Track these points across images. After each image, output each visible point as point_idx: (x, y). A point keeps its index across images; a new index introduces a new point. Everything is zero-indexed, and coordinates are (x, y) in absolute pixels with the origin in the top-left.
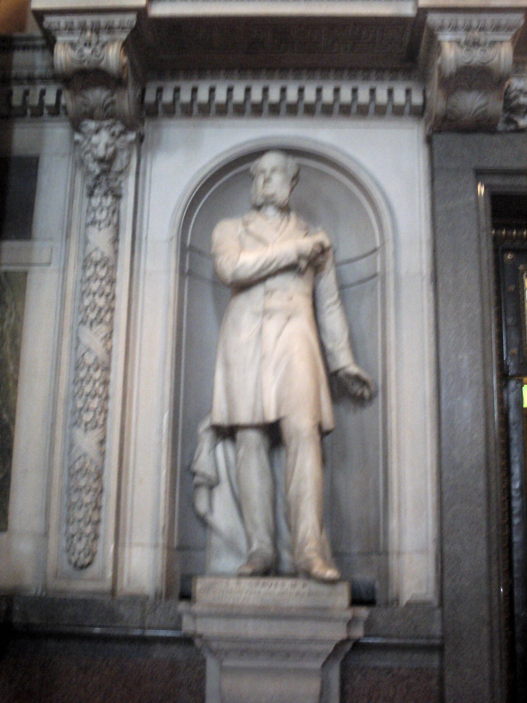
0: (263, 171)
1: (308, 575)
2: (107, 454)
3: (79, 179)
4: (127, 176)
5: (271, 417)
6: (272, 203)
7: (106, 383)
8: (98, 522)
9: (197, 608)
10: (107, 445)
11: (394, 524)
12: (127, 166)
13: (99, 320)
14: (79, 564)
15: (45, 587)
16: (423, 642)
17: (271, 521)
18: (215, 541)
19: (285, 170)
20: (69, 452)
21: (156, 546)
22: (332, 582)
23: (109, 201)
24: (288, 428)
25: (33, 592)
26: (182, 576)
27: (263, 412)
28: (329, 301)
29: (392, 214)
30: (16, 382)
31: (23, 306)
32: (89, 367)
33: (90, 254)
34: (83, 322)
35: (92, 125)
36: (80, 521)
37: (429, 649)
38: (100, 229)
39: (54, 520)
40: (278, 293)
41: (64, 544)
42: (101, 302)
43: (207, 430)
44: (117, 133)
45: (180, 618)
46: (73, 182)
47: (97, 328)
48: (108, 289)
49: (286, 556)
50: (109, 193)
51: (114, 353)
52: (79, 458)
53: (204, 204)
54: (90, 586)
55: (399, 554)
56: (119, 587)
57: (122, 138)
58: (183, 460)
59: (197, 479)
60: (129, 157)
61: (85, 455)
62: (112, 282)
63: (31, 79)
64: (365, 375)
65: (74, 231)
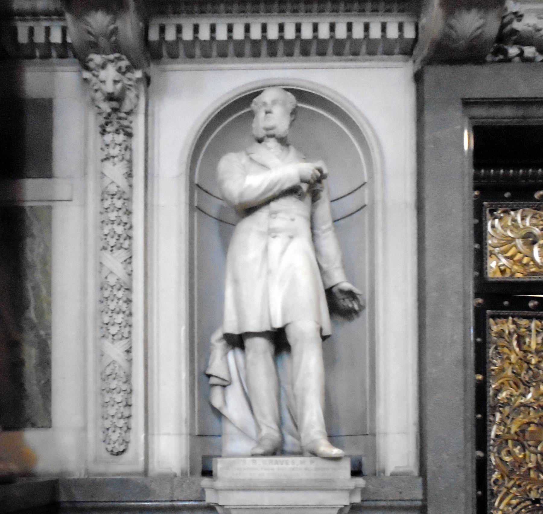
0: (265, 104)
1: (314, 454)
2: (134, 361)
4: (136, 114)
5: (278, 324)
6: (273, 136)
7: (129, 301)
8: (129, 417)
9: (219, 484)
10: (134, 354)
11: (380, 411)
12: (136, 106)
13: (119, 245)
14: (115, 451)
15: (87, 471)
16: (408, 504)
17: (277, 411)
18: (229, 428)
19: (284, 104)
20: (100, 361)
23: (121, 138)
24: (292, 336)
25: (77, 476)
27: (270, 320)
28: (324, 227)
30: (49, 304)
31: (50, 240)
32: (112, 287)
33: (107, 187)
34: (104, 248)
35: (97, 59)
36: (113, 416)
38: (114, 164)
39: (91, 416)
40: (281, 215)
41: (101, 436)
42: (119, 229)
43: (219, 340)
44: (124, 70)
45: (203, 490)
47: (117, 253)
48: (125, 219)
49: (289, 439)
50: (121, 131)
52: (109, 365)
55: (385, 434)
56: (150, 467)
57: (129, 75)
58: (199, 367)
59: (213, 381)
60: (137, 97)
61: (114, 362)
62: (129, 213)
63: (35, 15)
64: (356, 290)
65: (91, 169)
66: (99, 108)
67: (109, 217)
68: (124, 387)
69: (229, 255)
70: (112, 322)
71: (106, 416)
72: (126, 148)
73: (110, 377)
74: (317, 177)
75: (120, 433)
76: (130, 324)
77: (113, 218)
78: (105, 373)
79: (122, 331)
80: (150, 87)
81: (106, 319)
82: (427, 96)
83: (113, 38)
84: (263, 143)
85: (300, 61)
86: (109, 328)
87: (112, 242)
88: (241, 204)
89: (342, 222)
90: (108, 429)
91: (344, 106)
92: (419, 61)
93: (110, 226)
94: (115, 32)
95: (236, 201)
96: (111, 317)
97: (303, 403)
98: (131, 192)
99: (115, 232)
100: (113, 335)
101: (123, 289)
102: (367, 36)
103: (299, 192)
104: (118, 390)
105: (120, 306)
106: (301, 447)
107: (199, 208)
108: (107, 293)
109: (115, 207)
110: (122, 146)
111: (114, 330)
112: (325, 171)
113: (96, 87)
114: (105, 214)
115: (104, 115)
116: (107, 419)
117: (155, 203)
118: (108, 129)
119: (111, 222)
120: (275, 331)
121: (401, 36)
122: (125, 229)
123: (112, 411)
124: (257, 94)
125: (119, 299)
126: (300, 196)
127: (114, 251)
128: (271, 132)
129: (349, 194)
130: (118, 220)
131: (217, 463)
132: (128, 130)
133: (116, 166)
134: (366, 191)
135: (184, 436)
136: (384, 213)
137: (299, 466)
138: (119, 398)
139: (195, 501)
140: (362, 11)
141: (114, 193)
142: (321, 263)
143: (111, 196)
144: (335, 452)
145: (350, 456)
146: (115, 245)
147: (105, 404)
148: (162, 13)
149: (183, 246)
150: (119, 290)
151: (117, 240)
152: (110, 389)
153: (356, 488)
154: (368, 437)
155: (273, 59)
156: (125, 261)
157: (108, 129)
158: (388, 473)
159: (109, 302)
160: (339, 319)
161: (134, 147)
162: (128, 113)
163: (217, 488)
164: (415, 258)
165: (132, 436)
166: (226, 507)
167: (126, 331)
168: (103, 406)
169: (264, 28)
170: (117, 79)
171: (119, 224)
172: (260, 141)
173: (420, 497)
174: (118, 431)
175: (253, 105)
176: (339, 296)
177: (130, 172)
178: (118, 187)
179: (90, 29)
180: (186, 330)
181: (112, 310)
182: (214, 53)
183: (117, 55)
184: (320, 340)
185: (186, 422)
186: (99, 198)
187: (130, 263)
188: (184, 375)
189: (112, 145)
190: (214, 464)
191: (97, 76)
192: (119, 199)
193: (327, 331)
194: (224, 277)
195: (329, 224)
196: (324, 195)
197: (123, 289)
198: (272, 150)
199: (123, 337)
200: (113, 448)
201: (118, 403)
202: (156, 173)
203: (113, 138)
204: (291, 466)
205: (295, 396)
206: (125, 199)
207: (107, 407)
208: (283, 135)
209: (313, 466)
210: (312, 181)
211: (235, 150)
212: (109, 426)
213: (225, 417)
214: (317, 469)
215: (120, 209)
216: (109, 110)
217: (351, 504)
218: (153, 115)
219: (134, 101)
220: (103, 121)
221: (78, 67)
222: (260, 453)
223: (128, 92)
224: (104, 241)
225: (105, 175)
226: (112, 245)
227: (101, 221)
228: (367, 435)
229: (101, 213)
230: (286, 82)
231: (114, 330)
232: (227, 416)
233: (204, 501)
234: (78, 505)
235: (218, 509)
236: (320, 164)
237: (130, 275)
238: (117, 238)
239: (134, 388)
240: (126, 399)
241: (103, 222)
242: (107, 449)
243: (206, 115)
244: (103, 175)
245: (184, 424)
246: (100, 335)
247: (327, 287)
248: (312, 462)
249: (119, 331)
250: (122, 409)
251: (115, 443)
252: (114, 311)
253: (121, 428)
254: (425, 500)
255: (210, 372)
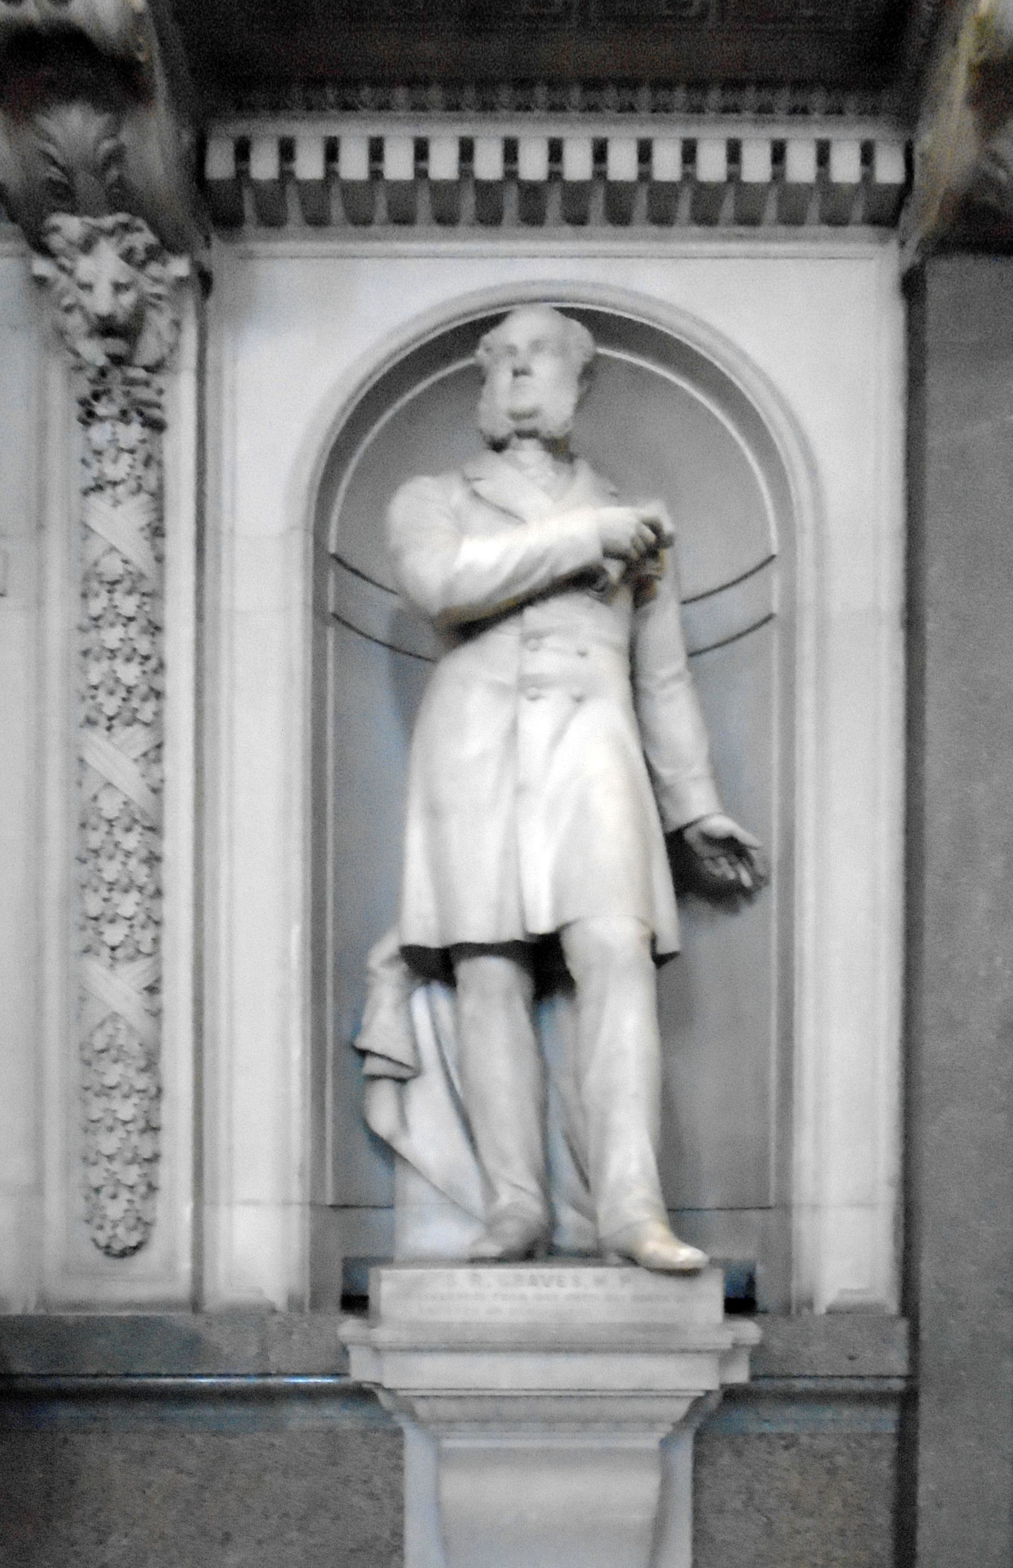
0: (512, 350)
1: (630, 1259)
3: (56, 378)
4: (176, 372)
5: (542, 924)
6: (532, 434)
7: (153, 860)
8: (154, 1159)
9: (383, 1335)
11: (804, 1150)
12: (174, 348)
13: (127, 715)
14: (117, 1247)
15: (43, 1300)
16: (869, 1385)
18: (413, 1189)
19: (562, 351)
21: (286, 1203)
22: (687, 1273)
23: (133, 433)
26: (346, 1260)
27: (522, 914)
28: (664, 673)
29: (813, 470)
32: (110, 822)
33: (96, 564)
34: (90, 722)
36: (110, 1158)
37: (882, 1398)
40: (550, 642)
41: (81, 1206)
42: (130, 673)
43: (391, 961)
44: (140, 256)
46: (43, 385)
47: (122, 733)
48: (144, 645)
49: (568, 1216)
50: (134, 415)
51: (169, 791)
52: (101, 1025)
53: (357, 472)
54: (143, 1292)
55: (815, 1207)
56: (208, 1287)
58: (337, 1030)
59: (373, 1065)
60: (177, 324)
61: (115, 1016)
62: (155, 629)
64: (744, 836)
65: (55, 514)
66: (77, 354)
67: (103, 641)
68: (142, 1082)
69: (417, 746)
70: (110, 913)
71: (92, 1157)
72: (148, 462)
73: (104, 1055)
74: (646, 543)
75: (130, 1201)
76: (156, 918)
77: (112, 643)
78: (92, 1045)
79: (137, 937)
80: (211, 303)
81: (94, 905)
82: (930, 338)
83: (113, 173)
84: (508, 453)
85: (606, 238)
86: (101, 930)
87: (111, 705)
88: (446, 613)
89: (706, 657)
90: (97, 1190)
91: (721, 359)
92: (912, 244)
93: (105, 665)
94: (116, 157)
95: (436, 607)
96: (105, 900)
97: (604, 1131)
98: (161, 576)
99: (117, 680)
100: (113, 949)
101: (138, 829)
102: (778, 175)
103: (601, 583)
104: (125, 1088)
105: (131, 872)
106: (598, 1241)
107: (336, 617)
108: (95, 839)
109: (119, 615)
110: (136, 456)
111: (114, 934)
112: (668, 527)
113: (67, 301)
114: (93, 634)
115: (91, 373)
116: (95, 1164)
117: (225, 603)
118: (101, 409)
119: (108, 654)
120: (534, 941)
121: (867, 178)
122: (144, 672)
123: (109, 1144)
124: (495, 321)
125: (128, 854)
126: (601, 594)
127: (114, 730)
128: (527, 425)
129: (734, 583)
130: (127, 650)
131: (379, 1280)
132: (155, 413)
133: (120, 508)
134: (775, 577)
135: (296, 1211)
136: (822, 635)
137: (593, 1290)
138: (126, 1110)
139: (323, 1375)
140: (764, 110)
141: (117, 578)
142: (654, 761)
143: (108, 587)
144: (686, 1255)
145: (725, 1264)
146: (118, 714)
147: (90, 1126)
148: (245, 108)
149: (299, 720)
150: (128, 830)
151: (124, 700)
152: (103, 1086)
153: (736, 1346)
154: (771, 1214)
155: (535, 230)
156: (145, 755)
157: (101, 409)
158: (821, 1309)
159: (102, 862)
160: (701, 907)
161: (168, 458)
162: (154, 369)
163: (379, 1346)
164: (899, 756)
165: (160, 1209)
166: (401, 1393)
167: (145, 937)
168: (86, 1131)
169: (511, 151)
170: (123, 280)
171: (128, 660)
172: (498, 446)
173: (901, 1367)
174: (125, 1195)
175: (480, 352)
176: (703, 850)
177: (156, 524)
178: (126, 562)
179: (52, 150)
180: (303, 933)
181: (110, 883)
182: (381, 212)
183: (122, 217)
184: (651, 964)
185: (301, 1175)
186: (75, 591)
187: (158, 760)
188: (298, 1051)
189: (112, 452)
190: (372, 1280)
191: (70, 272)
192: (130, 592)
193: (669, 944)
194: (403, 794)
195: (678, 663)
196: (664, 588)
197: (138, 829)
198: (532, 472)
199: (139, 952)
200: (111, 1238)
201: (125, 1123)
202: (225, 528)
203: (114, 434)
204: (569, 1289)
205: (583, 1110)
206: (144, 594)
207: (94, 1133)
208: (558, 434)
209: (626, 1291)
210: (634, 555)
211: (434, 470)
212: (102, 1182)
213: (404, 1160)
214: (638, 1298)
215: (131, 619)
216: (102, 361)
217: (722, 1386)
218: (219, 371)
219: (168, 337)
220: (85, 389)
221: (23, 246)
222: (494, 1255)
223: (151, 314)
224: (90, 702)
225: (92, 531)
226: (111, 714)
227: (84, 648)
228: (769, 1208)
229: (82, 630)
230: (564, 291)
231: (114, 934)
232: (407, 1158)
233: (347, 1375)
234: (20, 1384)
235: (381, 1395)
236: (654, 509)
237: (156, 791)
238: (124, 694)
239: (167, 1085)
240: (145, 1112)
241: (85, 653)
242: (94, 1240)
243: (340, 399)
244: (87, 531)
245: (295, 1178)
246: (76, 944)
247: (672, 828)
248: (624, 1280)
249: (127, 936)
250: (135, 1139)
251: (115, 1225)
252: (115, 887)
253: (132, 1187)
254: (912, 1377)
255: (364, 1042)
